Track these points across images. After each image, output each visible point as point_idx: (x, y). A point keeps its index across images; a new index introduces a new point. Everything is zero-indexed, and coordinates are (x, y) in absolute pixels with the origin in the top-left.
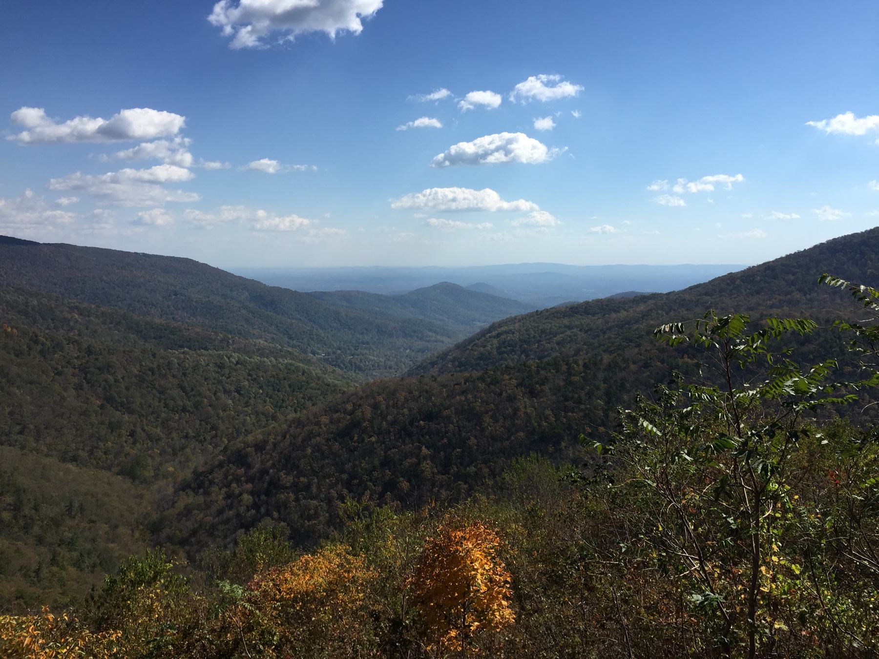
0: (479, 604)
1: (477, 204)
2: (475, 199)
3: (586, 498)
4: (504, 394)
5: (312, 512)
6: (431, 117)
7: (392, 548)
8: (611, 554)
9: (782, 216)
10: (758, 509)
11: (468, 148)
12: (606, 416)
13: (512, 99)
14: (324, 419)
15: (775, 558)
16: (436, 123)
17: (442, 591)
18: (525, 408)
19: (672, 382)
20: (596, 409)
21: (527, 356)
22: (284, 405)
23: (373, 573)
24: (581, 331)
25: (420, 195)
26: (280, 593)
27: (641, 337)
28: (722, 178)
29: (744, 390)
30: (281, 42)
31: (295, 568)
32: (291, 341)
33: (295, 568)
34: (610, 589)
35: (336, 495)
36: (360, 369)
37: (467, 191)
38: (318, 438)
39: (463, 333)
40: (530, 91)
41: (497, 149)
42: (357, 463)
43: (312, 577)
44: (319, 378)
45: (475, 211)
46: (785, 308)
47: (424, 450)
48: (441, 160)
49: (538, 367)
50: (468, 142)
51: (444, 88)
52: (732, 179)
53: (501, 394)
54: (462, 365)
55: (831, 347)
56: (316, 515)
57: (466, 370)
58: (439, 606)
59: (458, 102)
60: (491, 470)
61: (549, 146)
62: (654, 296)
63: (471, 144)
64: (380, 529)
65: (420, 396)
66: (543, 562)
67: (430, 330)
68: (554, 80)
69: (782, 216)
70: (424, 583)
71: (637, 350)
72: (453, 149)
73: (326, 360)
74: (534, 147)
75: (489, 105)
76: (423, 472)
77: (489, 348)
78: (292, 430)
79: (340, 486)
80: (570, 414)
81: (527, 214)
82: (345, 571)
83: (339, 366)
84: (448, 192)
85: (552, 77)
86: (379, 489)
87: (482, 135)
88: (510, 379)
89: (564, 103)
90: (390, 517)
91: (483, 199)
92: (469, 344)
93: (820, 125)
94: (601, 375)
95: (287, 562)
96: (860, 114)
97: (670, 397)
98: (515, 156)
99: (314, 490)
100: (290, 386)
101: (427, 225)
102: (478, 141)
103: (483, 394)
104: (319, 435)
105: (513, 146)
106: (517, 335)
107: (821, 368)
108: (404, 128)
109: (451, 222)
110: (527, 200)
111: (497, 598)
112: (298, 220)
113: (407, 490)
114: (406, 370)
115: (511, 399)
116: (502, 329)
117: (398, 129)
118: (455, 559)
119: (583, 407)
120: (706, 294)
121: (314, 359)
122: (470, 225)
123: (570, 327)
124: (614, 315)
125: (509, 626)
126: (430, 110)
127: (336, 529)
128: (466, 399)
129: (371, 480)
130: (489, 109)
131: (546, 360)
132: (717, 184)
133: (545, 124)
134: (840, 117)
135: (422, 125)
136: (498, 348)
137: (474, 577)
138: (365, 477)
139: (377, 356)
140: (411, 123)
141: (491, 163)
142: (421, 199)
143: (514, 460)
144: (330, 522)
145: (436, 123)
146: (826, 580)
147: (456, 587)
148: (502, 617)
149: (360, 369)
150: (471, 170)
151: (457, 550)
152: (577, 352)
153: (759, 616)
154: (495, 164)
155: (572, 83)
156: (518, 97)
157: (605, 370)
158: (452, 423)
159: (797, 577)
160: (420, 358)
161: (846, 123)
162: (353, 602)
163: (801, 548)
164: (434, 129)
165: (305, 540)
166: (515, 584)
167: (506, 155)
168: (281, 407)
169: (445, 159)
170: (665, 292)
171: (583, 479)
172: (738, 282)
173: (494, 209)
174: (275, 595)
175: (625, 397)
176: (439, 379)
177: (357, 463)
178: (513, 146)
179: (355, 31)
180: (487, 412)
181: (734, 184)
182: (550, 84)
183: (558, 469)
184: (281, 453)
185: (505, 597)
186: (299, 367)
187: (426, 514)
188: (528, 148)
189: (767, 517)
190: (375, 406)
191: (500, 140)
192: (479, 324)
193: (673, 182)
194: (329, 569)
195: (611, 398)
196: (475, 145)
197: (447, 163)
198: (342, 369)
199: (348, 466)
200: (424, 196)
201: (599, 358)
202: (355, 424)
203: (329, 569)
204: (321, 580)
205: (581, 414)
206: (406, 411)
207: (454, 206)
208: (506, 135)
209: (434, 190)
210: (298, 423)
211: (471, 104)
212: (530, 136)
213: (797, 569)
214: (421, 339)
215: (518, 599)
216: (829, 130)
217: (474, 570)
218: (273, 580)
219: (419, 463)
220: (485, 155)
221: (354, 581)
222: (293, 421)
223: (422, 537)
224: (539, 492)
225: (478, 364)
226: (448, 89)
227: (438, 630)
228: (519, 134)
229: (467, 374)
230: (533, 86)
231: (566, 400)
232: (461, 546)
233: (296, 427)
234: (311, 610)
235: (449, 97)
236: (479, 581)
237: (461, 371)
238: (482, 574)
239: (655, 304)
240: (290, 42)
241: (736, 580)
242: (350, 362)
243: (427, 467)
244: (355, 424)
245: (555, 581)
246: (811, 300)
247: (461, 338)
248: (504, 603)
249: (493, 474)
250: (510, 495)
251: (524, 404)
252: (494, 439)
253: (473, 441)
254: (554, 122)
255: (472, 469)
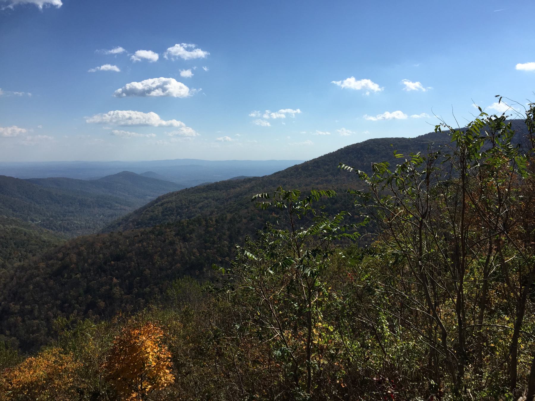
0: (151, 374)
1: (145, 122)
2: (144, 118)
3: (218, 301)
4: (167, 241)
5: (35, 328)
6: (112, 64)
7: (92, 346)
8: (232, 332)
9: (321, 133)
10: (310, 296)
11: (139, 86)
12: (230, 250)
13: (165, 57)
14: (42, 265)
15: (320, 324)
16: (116, 69)
17: (127, 367)
18: (181, 248)
19: (266, 228)
20: (223, 246)
21: (181, 217)
22: (11, 257)
23: (80, 364)
24: (213, 200)
25: (106, 115)
26: (12, 385)
27: (248, 203)
28: (289, 111)
29: (302, 231)
30: (3, 9)
31: (22, 368)
32: (15, 213)
33: (22, 368)
34: (233, 353)
35: (52, 315)
36: (68, 230)
37: (138, 113)
38: (38, 278)
39: (139, 203)
40: (176, 53)
41: (157, 88)
42: (67, 292)
43: (35, 372)
44: (37, 238)
45: (144, 126)
46: (324, 184)
47: (115, 280)
48: (120, 92)
49: (188, 223)
50: (138, 82)
51: (121, 46)
52: (295, 112)
53: (165, 241)
54: (139, 224)
55: (348, 205)
56: (38, 330)
57: (142, 227)
58: (125, 379)
59: (130, 57)
60: (160, 289)
61: (190, 87)
62: (255, 179)
63: (140, 84)
64: (83, 335)
65: (111, 245)
66: (193, 342)
67: (117, 202)
68: (192, 47)
69: (321, 133)
70: (114, 366)
71: (246, 210)
72: (128, 86)
73: (41, 225)
74: (181, 88)
75: (150, 60)
76: (114, 294)
77: (156, 212)
78: (18, 274)
79: (55, 309)
80: (208, 251)
81: (178, 128)
82: (59, 365)
83: (52, 229)
84: (126, 113)
85: (190, 45)
86: (84, 308)
87: (147, 78)
88: (171, 231)
89: (197, 61)
90: (90, 326)
91: (149, 119)
92: (143, 210)
93: (338, 83)
94: (226, 226)
95: (16, 364)
96: (358, 78)
97: (265, 237)
98: (169, 92)
99: (36, 313)
100: (15, 244)
101: (112, 134)
102: (145, 82)
103: (153, 242)
104: (38, 276)
105: (168, 86)
106: (174, 203)
107: (340, 216)
108: (93, 70)
109: (128, 133)
110: (177, 120)
111: (163, 369)
112: (18, 130)
113: (103, 307)
114: (101, 229)
115: (172, 243)
116: (165, 200)
117: (89, 71)
118: (134, 348)
119: (216, 246)
120: (284, 177)
121: (33, 224)
122: (141, 135)
123: (206, 198)
124: (232, 190)
125: (171, 384)
126: (112, 60)
127: (53, 337)
128: (143, 246)
129: (77, 303)
130: (151, 62)
131: (193, 218)
132: (287, 114)
133: (187, 73)
134: (348, 79)
135: (106, 69)
136: (162, 212)
137: (147, 358)
138: (73, 302)
139: (80, 221)
140: (98, 68)
141: (152, 96)
142: (107, 117)
143: (173, 281)
144: (48, 334)
145: (116, 69)
146: (347, 333)
147: (136, 365)
148: (166, 380)
149: (68, 230)
150: (141, 100)
151: (135, 342)
152: (212, 213)
153: (313, 357)
154: (156, 97)
155: (202, 50)
156: (169, 56)
157: (229, 223)
158: (134, 262)
159: (332, 333)
160: (110, 220)
161: (351, 83)
162: (65, 384)
163: (334, 316)
164: (115, 72)
165: (30, 347)
166: (174, 359)
167: (163, 92)
168: (9, 258)
169: (123, 92)
170: (261, 176)
171: (217, 289)
172: (300, 170)
173: (157, 125)
174: (8, 386)
175: (240, 238)
176: (123, 234)
177: (67, 292)
178: (168, 86)
179: (57, 5)
180: (156, 253)
181: (296, 114)
182: (189, 49)
183: (201, 285)
184: (10, 290)
185: (168, 368)
186: (22, 230)
187: (116, 321)
188: (177, 88)
189: (316, 301)
190: (79, 254)
191: (159, 82)
192: (149, 198)
193: (263, 112)
194: (48, 365)
195: (232, 239)
196: (142, 84)
197: (124, 95)
198: (54, 230)
199: (61, 295)
200: (109, 115)
201: (225, 216)
202: (65, 267)
203: (48, 365)
204: (42, 373)
205: (215, 250)
206: (101, 256)
207: (130, 122)
208: (163, 79)
209: (116, 112)
210: (22, 268)
211: (139, 57)
212: (178, 80)
213: (331, 329)
214: (110, 208)
215: (177, 366)
216: (343, 86)
217: (147, 353)
218: (6, 377)
219: (111, 289)
220: (150, 91)
221: (66, 371)
222: (19, 267)
223: (112, 337)
224: (190, 299)
225: (149, 223)
226: (124, 48)
227: (124, 394)
228: (171, 79)
229: (142, 230)
230: (178, 50)
231: (206, 242)
232: (138, 340)
233: (21, 272)
234: (35, 393)
235: (124, 52)
236: (151, 360)
237: (138, 228)
238: (152, 355)
239: (255, 183)
240: (10, 9)
241: (300, 338)
242: (60, 225)
243: (117, 291)
244: (65, 267)
245: (200, 353)
246: (337, 180)
247: (138, 207)
248: (167, 371)
249: (161, 291)
250: (172, 303)
251: (180, 247)
252: (161, 269)
253: (148, 271)
254: (192, 73)
255: (148, 289)
